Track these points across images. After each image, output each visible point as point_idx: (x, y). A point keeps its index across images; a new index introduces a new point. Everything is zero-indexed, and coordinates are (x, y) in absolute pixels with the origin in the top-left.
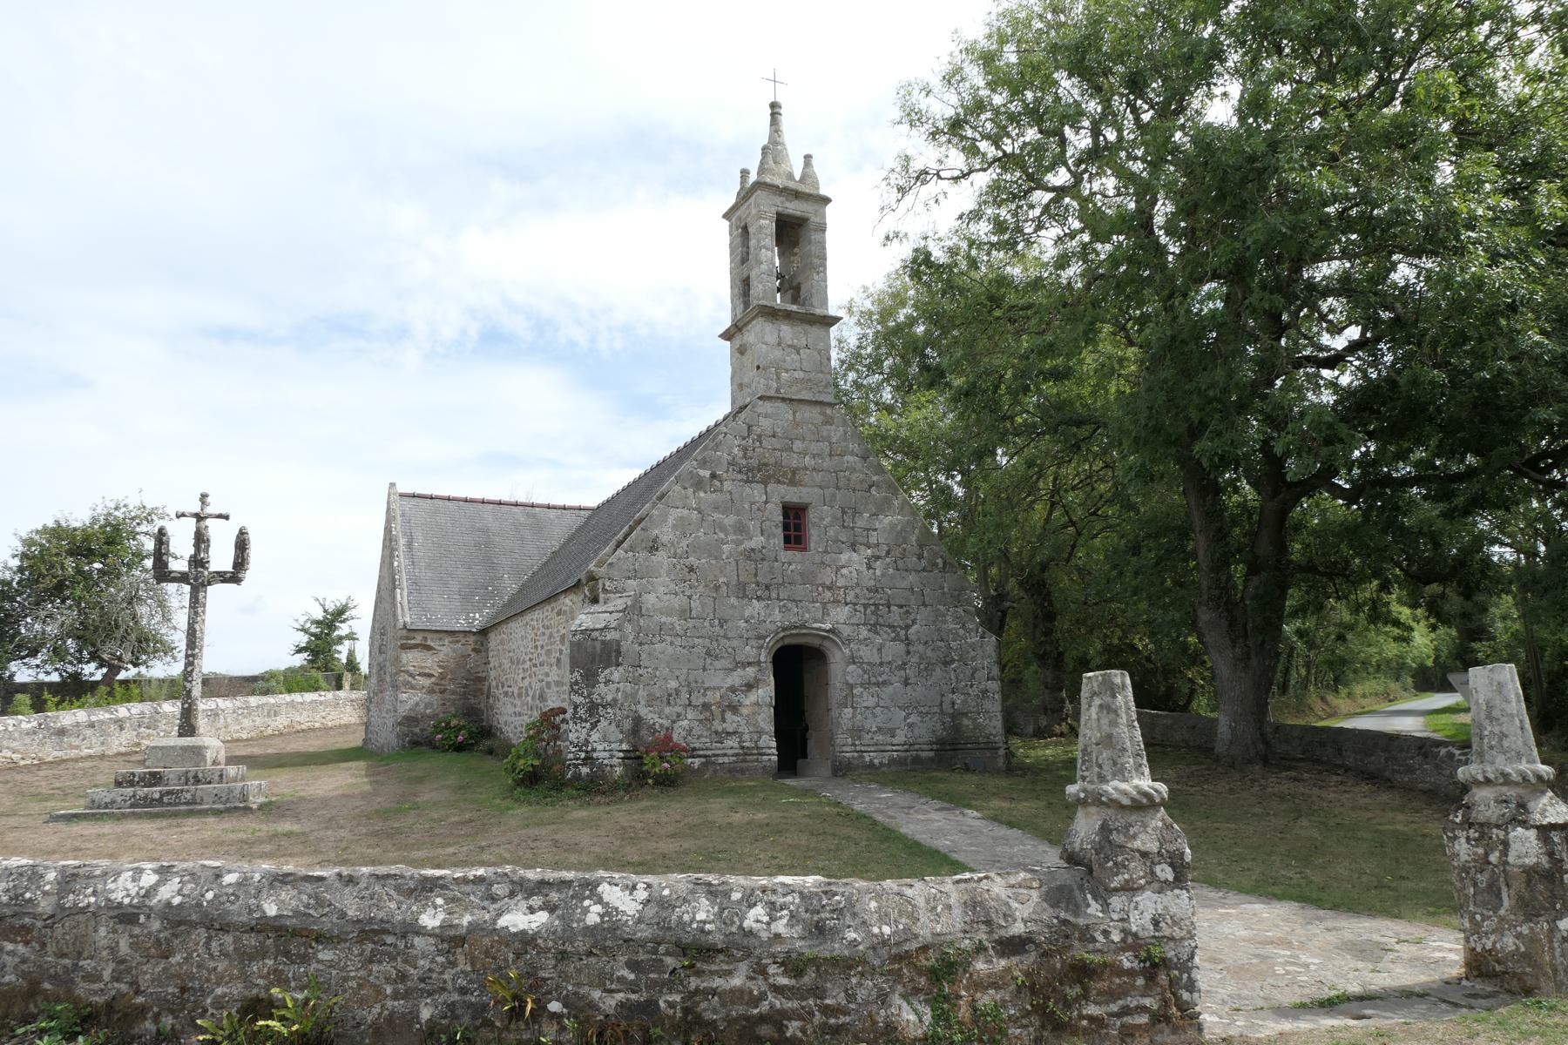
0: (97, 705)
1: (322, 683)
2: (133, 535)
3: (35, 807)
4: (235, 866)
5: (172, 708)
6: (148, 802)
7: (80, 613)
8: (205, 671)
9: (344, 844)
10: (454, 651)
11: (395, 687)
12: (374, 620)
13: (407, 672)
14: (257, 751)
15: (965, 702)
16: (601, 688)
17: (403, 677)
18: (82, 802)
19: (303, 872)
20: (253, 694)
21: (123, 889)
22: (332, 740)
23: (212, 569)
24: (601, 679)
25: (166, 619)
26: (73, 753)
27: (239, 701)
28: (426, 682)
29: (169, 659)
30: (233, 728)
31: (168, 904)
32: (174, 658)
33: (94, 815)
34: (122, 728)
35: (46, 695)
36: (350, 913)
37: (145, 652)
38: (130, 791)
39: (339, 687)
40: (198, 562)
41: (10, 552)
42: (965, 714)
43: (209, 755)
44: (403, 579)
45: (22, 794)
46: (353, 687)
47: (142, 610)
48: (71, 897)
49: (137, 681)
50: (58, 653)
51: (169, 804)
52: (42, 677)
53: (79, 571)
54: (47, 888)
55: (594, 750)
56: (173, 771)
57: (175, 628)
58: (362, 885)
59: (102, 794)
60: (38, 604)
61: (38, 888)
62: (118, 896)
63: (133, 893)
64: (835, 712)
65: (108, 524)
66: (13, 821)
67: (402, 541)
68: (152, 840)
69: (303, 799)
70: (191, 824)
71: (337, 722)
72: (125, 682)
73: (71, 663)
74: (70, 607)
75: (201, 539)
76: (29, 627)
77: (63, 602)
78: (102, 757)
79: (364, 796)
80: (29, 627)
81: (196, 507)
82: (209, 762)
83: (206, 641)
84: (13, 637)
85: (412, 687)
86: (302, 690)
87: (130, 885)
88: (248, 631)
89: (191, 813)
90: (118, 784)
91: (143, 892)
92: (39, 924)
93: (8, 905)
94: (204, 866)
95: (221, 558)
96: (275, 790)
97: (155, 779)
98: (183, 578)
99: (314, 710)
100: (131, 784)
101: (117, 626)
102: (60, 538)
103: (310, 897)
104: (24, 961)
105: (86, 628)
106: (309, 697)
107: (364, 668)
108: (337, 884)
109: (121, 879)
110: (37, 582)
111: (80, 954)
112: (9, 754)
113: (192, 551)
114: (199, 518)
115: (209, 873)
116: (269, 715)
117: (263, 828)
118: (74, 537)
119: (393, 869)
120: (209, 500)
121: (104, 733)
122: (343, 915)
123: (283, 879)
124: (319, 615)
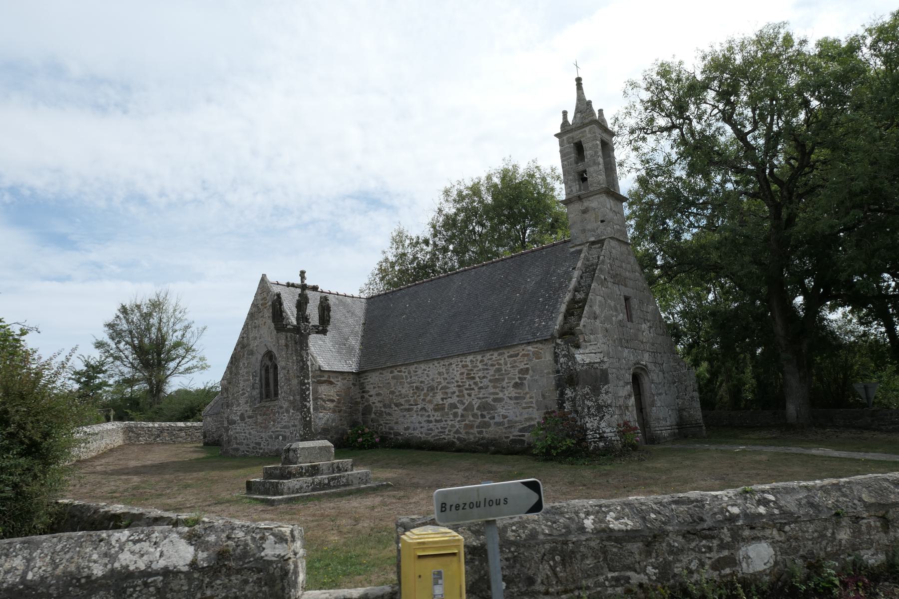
10: (344, 385)
13: (321, 399)
15: (683, 403)
16: (603, 397)
24: (603, 391)
28: (330, 405)
42: (684, 410)
51: (334, 487)
55: (604, 432)
64: (648, 410)
85: (325, 409)
120: (306, 275)
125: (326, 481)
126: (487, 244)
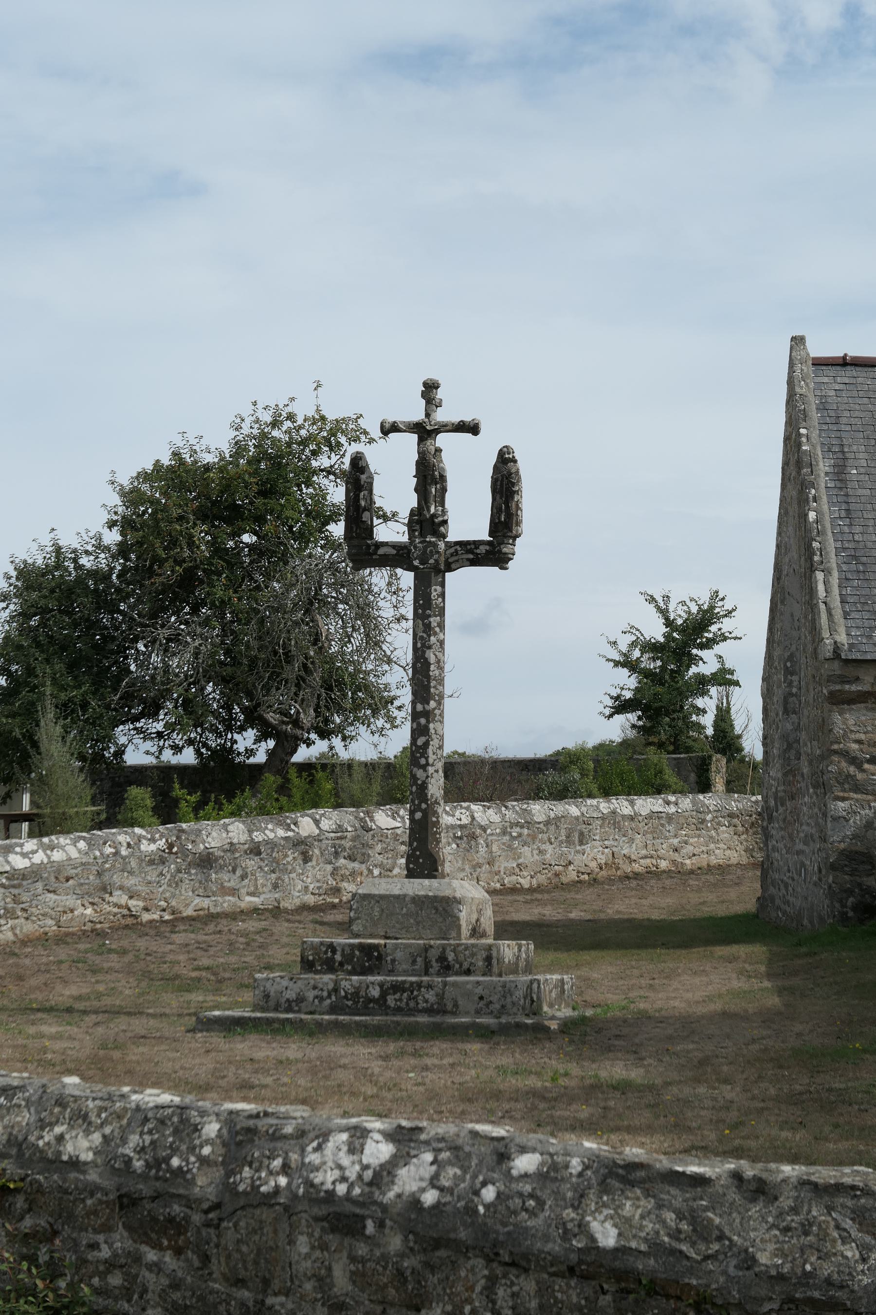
0: (263, 811)
1: (670, 777)
2: (307, 475)
3: (172, 1001)
4: (533, 1139)
5: (389, 820)
6: (359, 1002)
7: (224, 634)
8: (448, 749)
9: (733, 1116)
11: (821, 786)
12: (771, 641)
13: (845, 754)
14: (550, 913)
17: (838, 766)
18: (248, 996)
19: (663, 1163)
20: (536, 795)
21: (334, 1165)
22: (694, 898)
23: (452, 537)
25: (373, 641)
26: (227, 903)
27: (512, 811)
29: (380, 722)
30: (505, 864)
31: (415, 1203)
32: (391, 720)
33: (269, 1022)
34: (306, 859)
35: (178, 791)
36: (763, 1258)
37: (340, 710)
38: (327, 979)
39: (705, 786)
40: (426, 521)
41: (105, 517)
43: (465, 916)
44: (829, 546)
45: (147, 974)
46: (731, 787)
47: (331, 626)
48: (247, 1172)
49: (326, 766)
50: (192, 711)
51: (398, 1010)
52: (168, 756)
53: (217, 549)
54: (206, 1151)
56: (403, 944)
57: (389, 661)
58: (786, 1202)
59: (281, 983)
60: (154, 616)
61: (192, 1149)
62: (327, 1178)
63: (352, 1173)
65: (262, 455)
66: (138, 1025)
67: (824, 466)
68: (371, 1079)
69: (644, 1017)
70: (439, 1052)
71: (703, 861)
72: (306, 767)
73: (214, 730)
74: (206, 622)
75: (429, 477)
76: (144, 660)
77: (195, 610)
78: (276, 912)
79: (768, 1018)
80: (144, 660)
81: (416, 412)
82: (465, 931)
83: (449, 686)
84: (118, 679)
86: (631, 790)
87: (345, 1160)
88: (523, 666)
89: (438, 1032)
90: (308, 965)
91: (368, 1175)
92: (197, 1218)
93: (144, 1177)
94: (475, 1134)
95: (467, 516)
96: (590, 995)
97: (370, 959)
98: (398, 557)
99: (656, 833)
100: (330, 966)
101: (289, 658)
102: (182, 487)
103: (680, 1216)
104: (176, 1285)
105: (236, 662)
106: (646, 805)
107: (753, 745)
108: (733, 1195)
109: (330, 1145)
110: (151, 572)
111: (266, 1282)
112: (124, 899)
113: (413, 501)
114: (424, 432)
115: (485, 1149)
116: (569, 841)
117: (575, 1071)
118: (207, 482)
119: (848, 1175)
120: (440, 394)
121: (277, 867)
122: (748, 1261)
123: (620, 1176)
124: (656, 631)
125: (375, 992)
126: (157, 495)
